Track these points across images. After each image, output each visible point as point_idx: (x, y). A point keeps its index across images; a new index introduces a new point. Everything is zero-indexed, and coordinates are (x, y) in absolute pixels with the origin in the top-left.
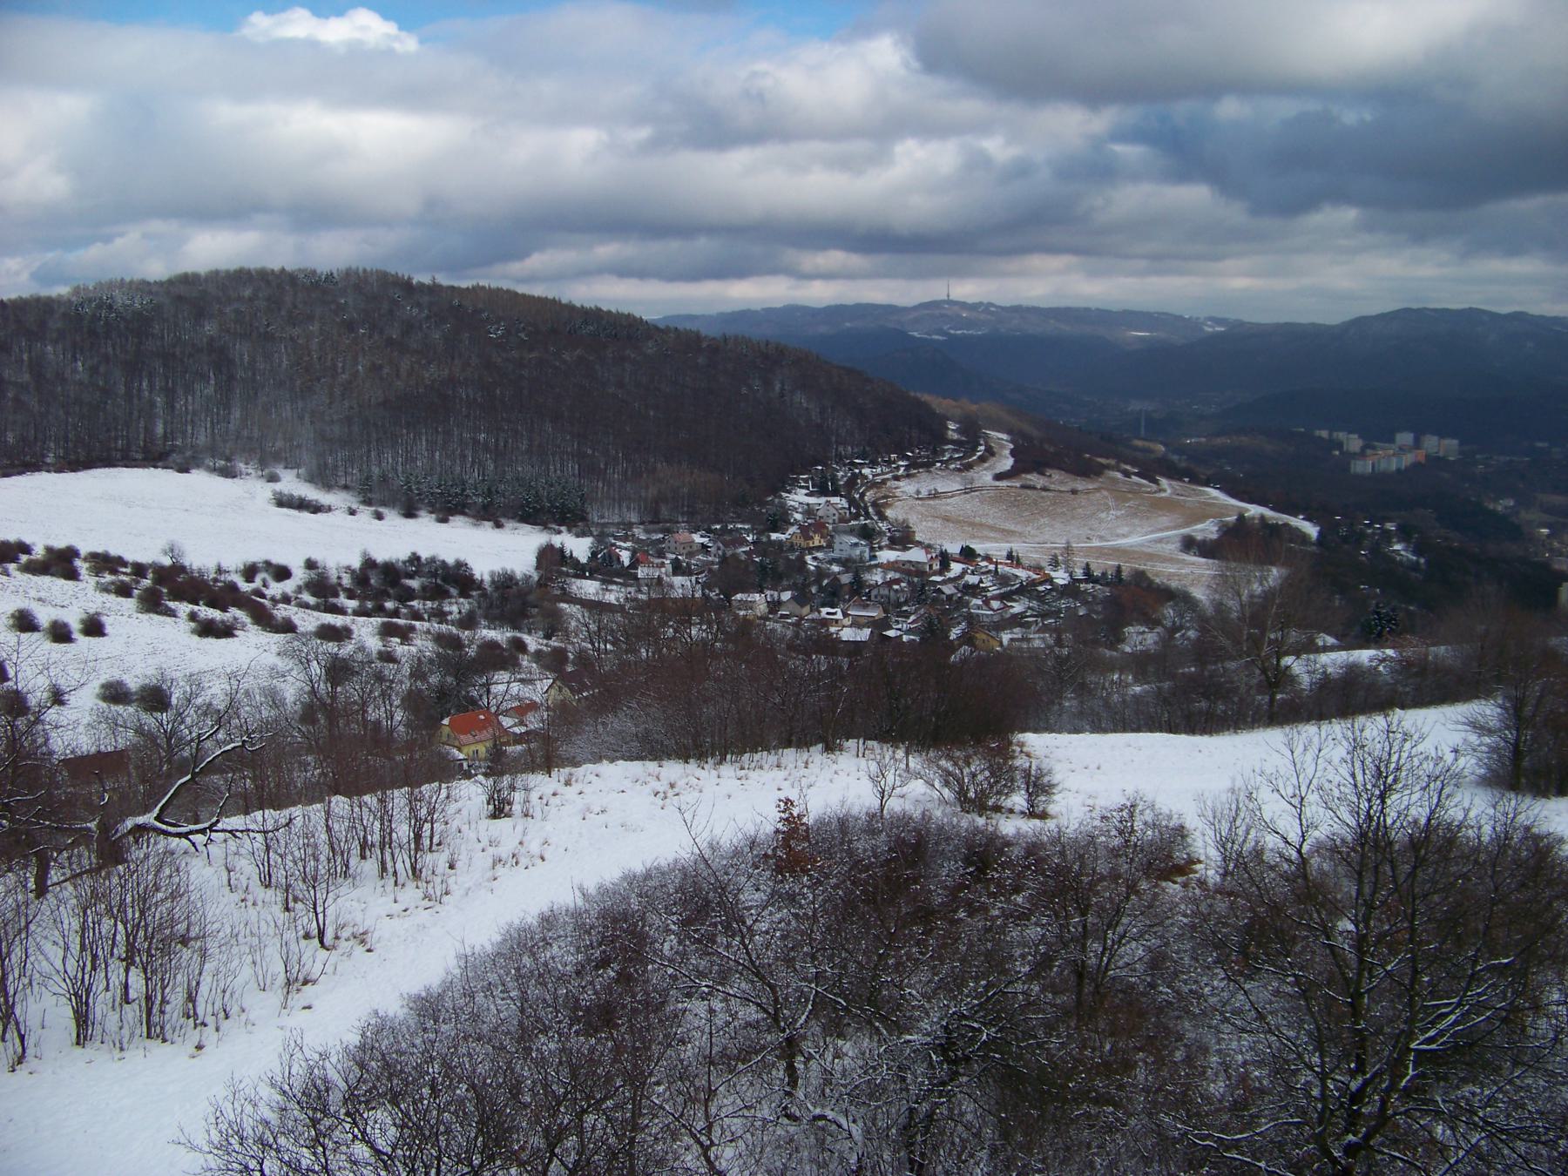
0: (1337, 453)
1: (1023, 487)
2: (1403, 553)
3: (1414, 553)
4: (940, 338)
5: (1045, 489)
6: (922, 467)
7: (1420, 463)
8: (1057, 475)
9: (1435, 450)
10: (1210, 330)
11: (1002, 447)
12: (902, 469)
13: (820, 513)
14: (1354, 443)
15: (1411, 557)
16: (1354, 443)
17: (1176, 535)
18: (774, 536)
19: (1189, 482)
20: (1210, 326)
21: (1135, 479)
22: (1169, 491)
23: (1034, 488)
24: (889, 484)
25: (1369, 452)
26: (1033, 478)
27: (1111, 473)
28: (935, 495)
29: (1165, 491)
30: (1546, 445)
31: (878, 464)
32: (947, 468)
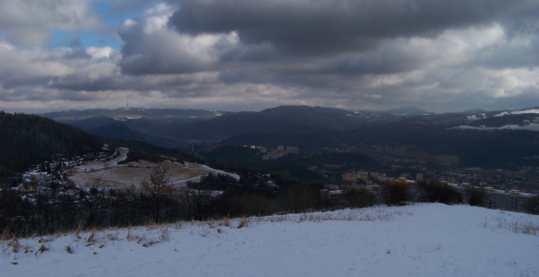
0: (258, 153)
1: (128, 166)
2: (271, 184)
3: (276, 184)
4: (124, 120)
5: (137, 167)
6: (89, 161)
7: (286, 155)
8: (143, 162)
9: (291, 151)
10: (218, 115)
11: (124, 152)
12: (81, 161)
13: (37, 178)
14: (264, 150)
15: (274, 185)
16: (264, 150)
17: (184, 182)
18: (13, 188)
19: (197, 163)
20: (218, 114)
21: (175, 162)
22: (187, 166)
23: (133, 167)
24: (75, 167)
25: (268, 152)
26: (135, 164)
27: (167, 161)
28: (93, 171)
29: (186, 166)
30: (327, 148)
31: (72, 160)
32: (99, 160)
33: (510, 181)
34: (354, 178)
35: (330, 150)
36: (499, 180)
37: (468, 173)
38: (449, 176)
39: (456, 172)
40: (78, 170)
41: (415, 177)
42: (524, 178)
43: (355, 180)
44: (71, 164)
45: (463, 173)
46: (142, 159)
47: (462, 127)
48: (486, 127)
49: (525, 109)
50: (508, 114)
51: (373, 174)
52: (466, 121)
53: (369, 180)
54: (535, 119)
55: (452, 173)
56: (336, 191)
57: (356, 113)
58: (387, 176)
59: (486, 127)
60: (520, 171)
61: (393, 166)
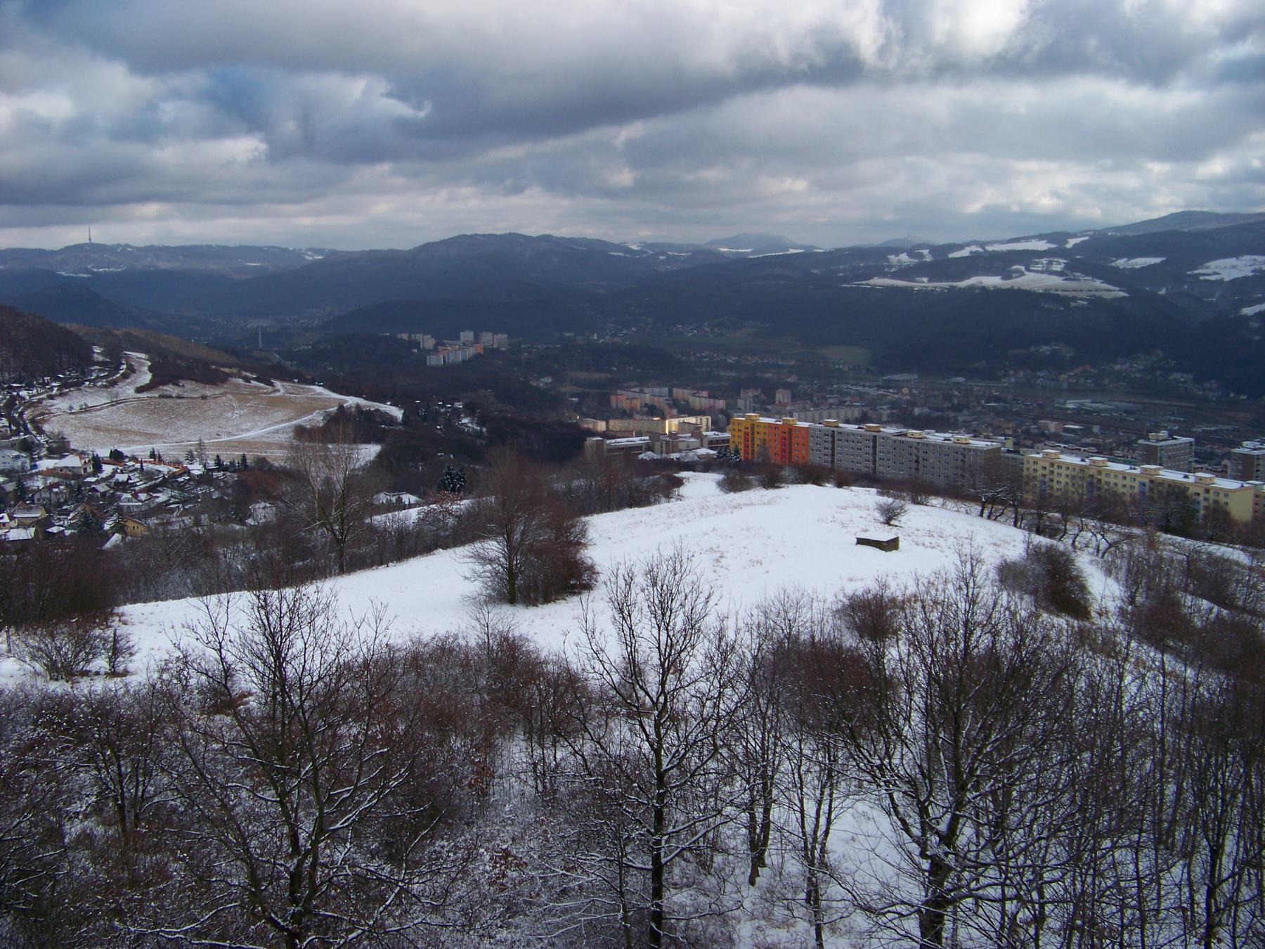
1: (161, 397)
3: (478, 424)
4: (85, 276)
5: (179, 397)
7: (480, 354)
8: (189, 385)
10: (310, 258)
11: (142, 364)
16: (428, 342)
21: (254, 383)
23: (170, 397)
26: (170, 389)
28: (86, 409)
29: (279, 391)
30: (572, 334)
31: (34, 386)
32: (95, 386)
33: (979, 404)
34: (637, 404)
35: (579, 338)
36: (956, 401)
37: (891, 388)
38: (847, 394)
39: (864, 386)
40: (53, 410)
41: (774, 397)
42: (1010, 397)
43: (639, 408)
44: (34, 396)
45: (879, 387)
46: (183, 378)
47: (877, 281)
48: (930, 281)
49: (1017, 240)
50: (980, 250)
51: (679, 393)
52: (887, 266)
53: (671, 407)
54: (1037, 263)
55: (854, 387)
56: (618, 440)
57: (634, 248)
58: (710, 397)
59: (930, 281)
60: (1003, 380)
61: (722, 373)
